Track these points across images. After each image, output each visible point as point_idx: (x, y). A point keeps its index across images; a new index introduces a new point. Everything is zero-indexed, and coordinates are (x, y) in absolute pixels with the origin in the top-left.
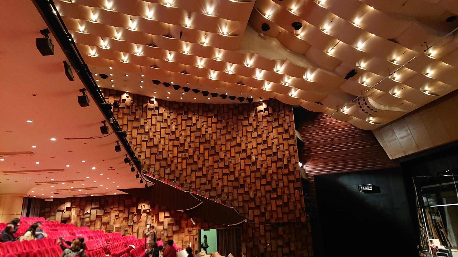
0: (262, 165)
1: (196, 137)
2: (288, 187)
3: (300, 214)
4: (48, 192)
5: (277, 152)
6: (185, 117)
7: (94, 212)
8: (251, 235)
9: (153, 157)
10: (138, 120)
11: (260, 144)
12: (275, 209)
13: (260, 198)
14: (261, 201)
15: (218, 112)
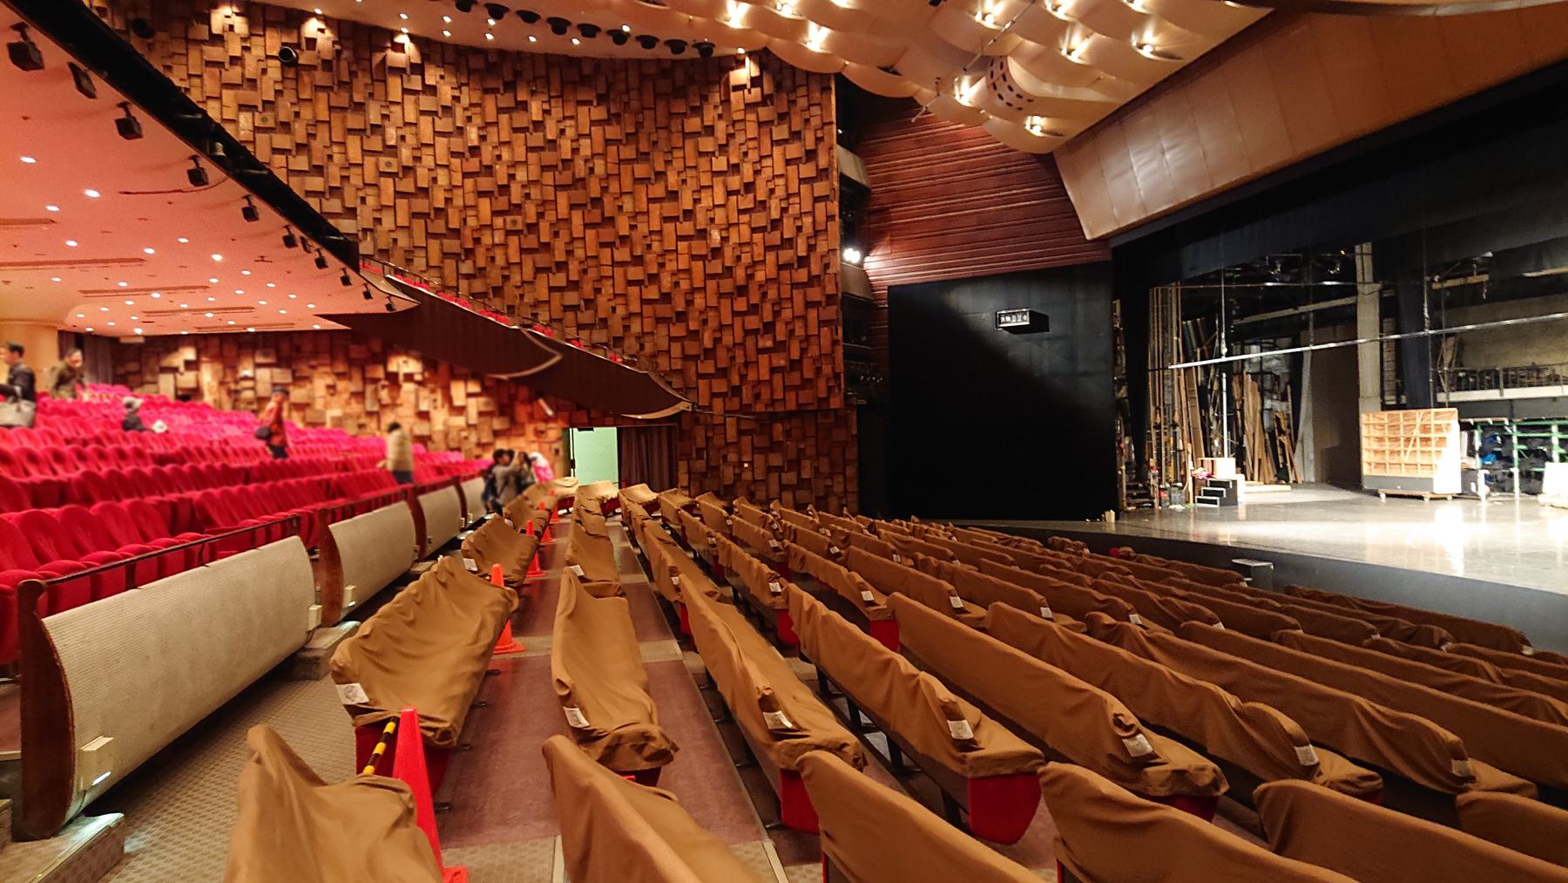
0: (739, 258)
1: (544, 168)
2: (804, 318)
3: (830, 389)
4: (126, 319)
5: (780, 220)
6: (506, 100)
7: (264, 375)
8: (701, 443)
9: (418, 225)
10: (359, 107)
11: (736, 193)
12: (767, 377)
13: (729, 350)
14: (733, 358)
15: (609, 86)
